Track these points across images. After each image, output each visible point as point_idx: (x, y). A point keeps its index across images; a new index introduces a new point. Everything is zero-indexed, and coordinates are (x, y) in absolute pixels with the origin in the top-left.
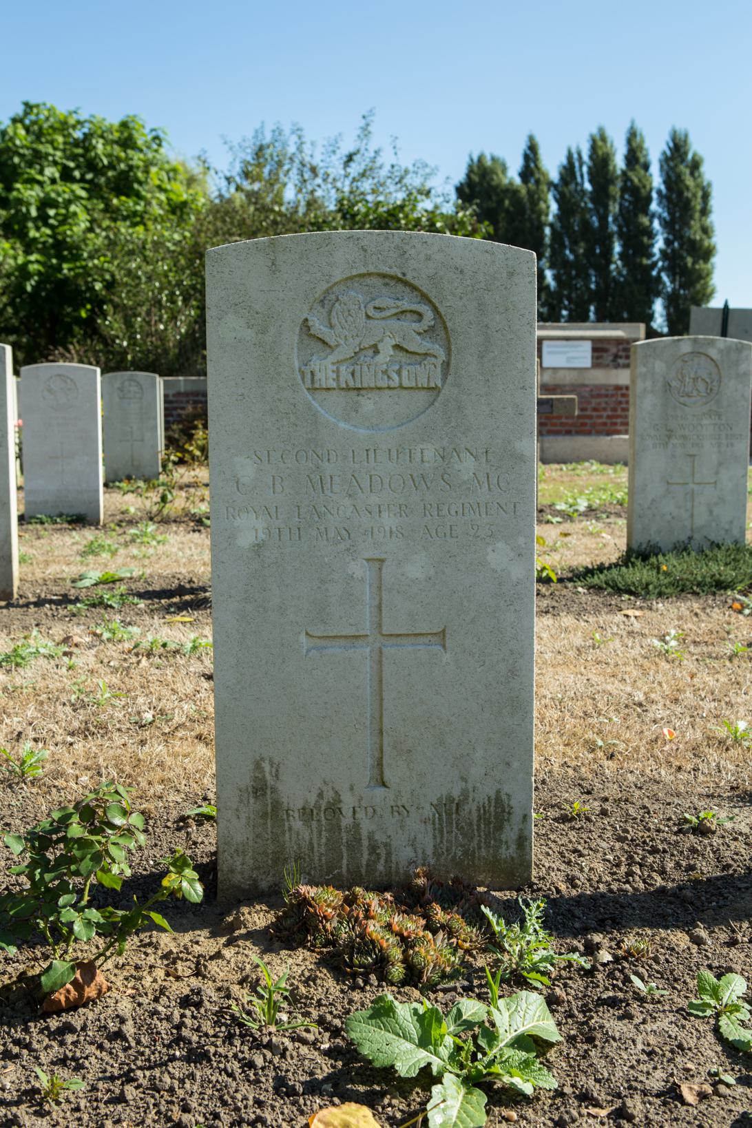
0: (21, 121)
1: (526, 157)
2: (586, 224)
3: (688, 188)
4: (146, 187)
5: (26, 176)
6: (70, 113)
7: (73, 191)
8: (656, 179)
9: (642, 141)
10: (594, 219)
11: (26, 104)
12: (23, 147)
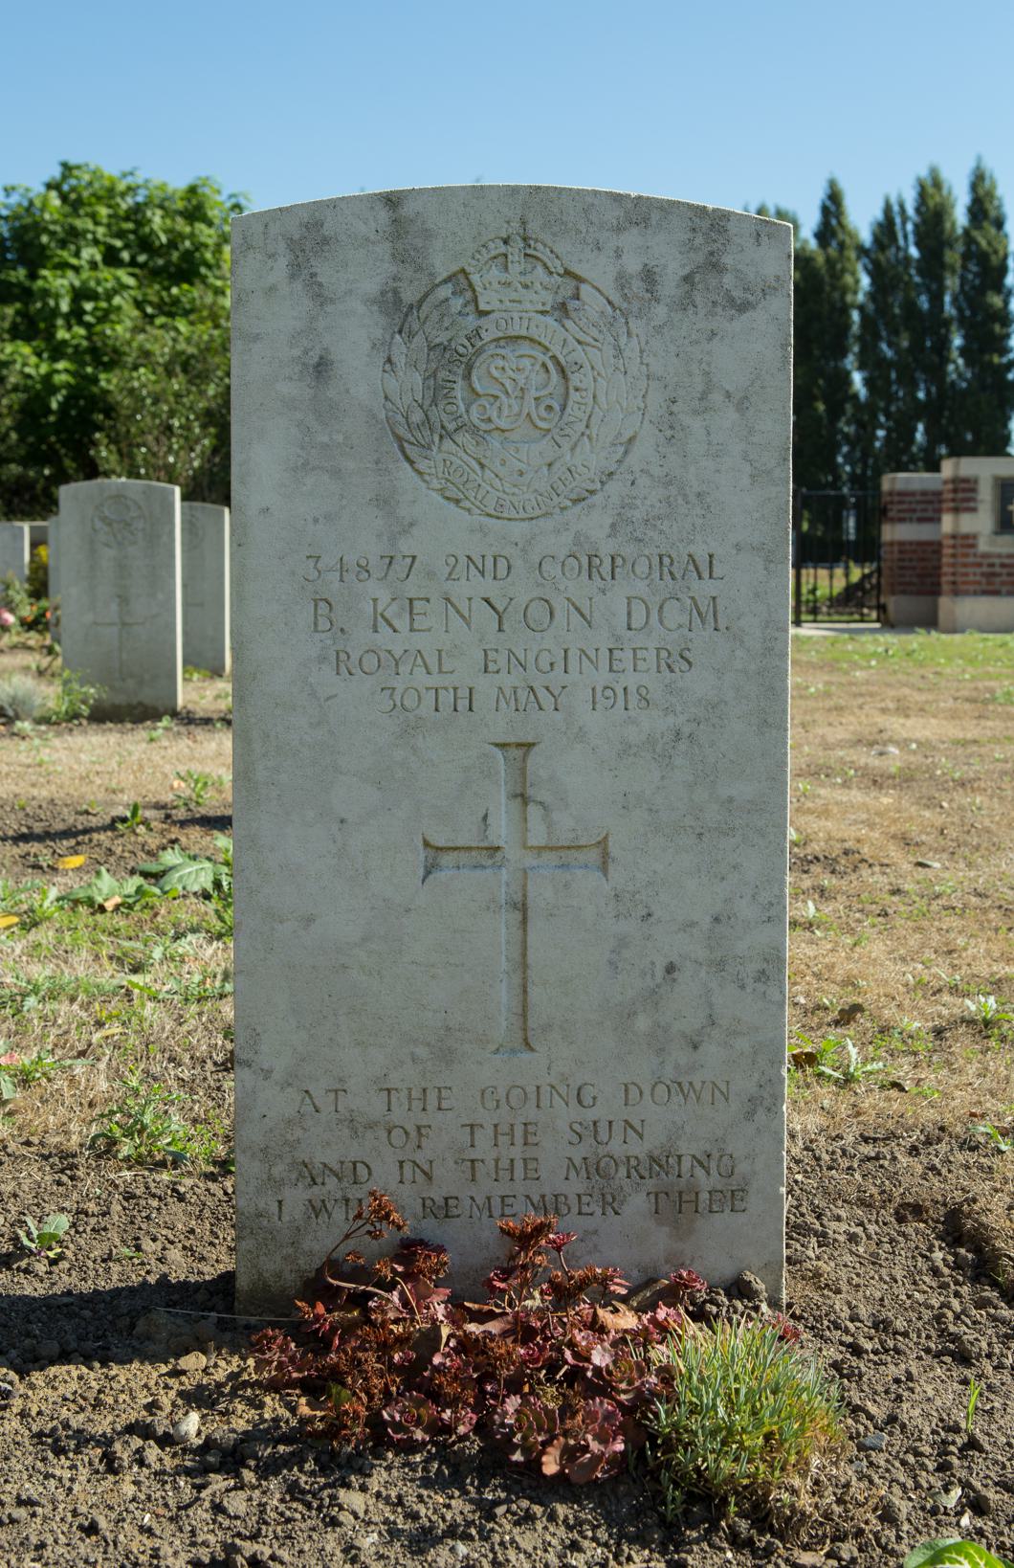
1: (825, 211)
2: (910, 307)
4: (218, 273)
5: (56, 260)
6: (124, 175)
7: (118, 279)
9: (994, 186)
12: (54, 222)
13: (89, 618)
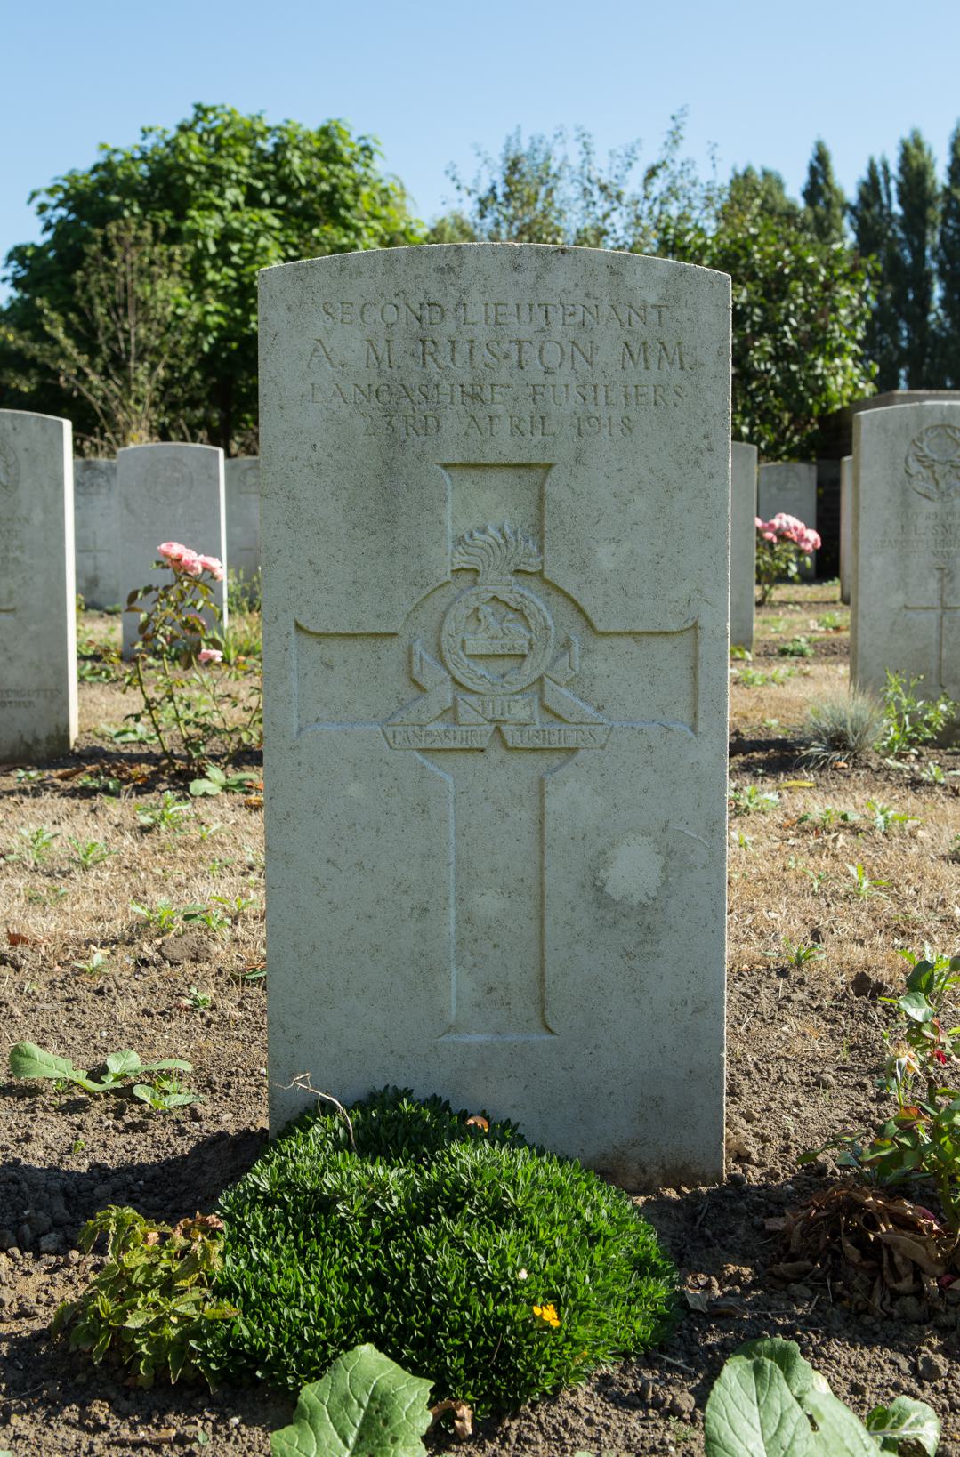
0: (191, 128)
1: (813, 171)
4: (354, 212)
5: (201, 200)
7: (261, 220)
10: (906, 252)
12: (199, 163)
13: (898, 599)
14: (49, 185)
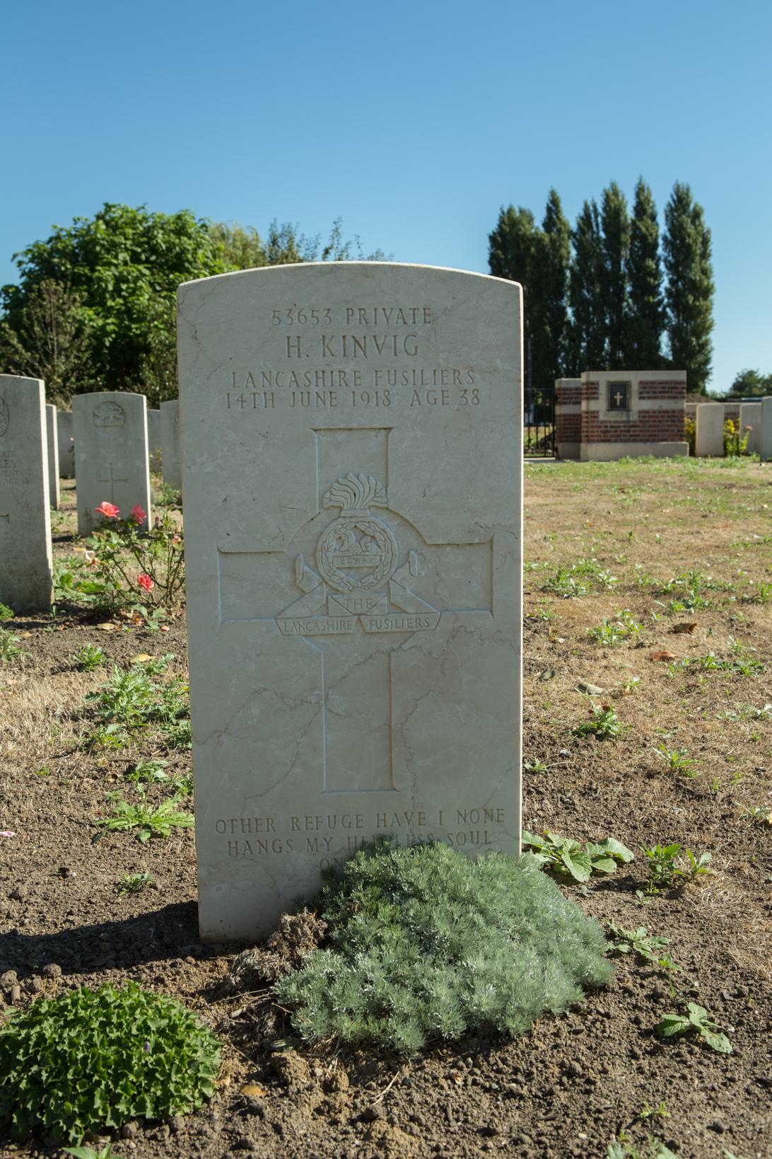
1: (549, 210)
2: (601, 268)
3: (689, 235)
8: (663, 229)
9: (650, 194)
11: (107, 205)
14: (24, 249)
